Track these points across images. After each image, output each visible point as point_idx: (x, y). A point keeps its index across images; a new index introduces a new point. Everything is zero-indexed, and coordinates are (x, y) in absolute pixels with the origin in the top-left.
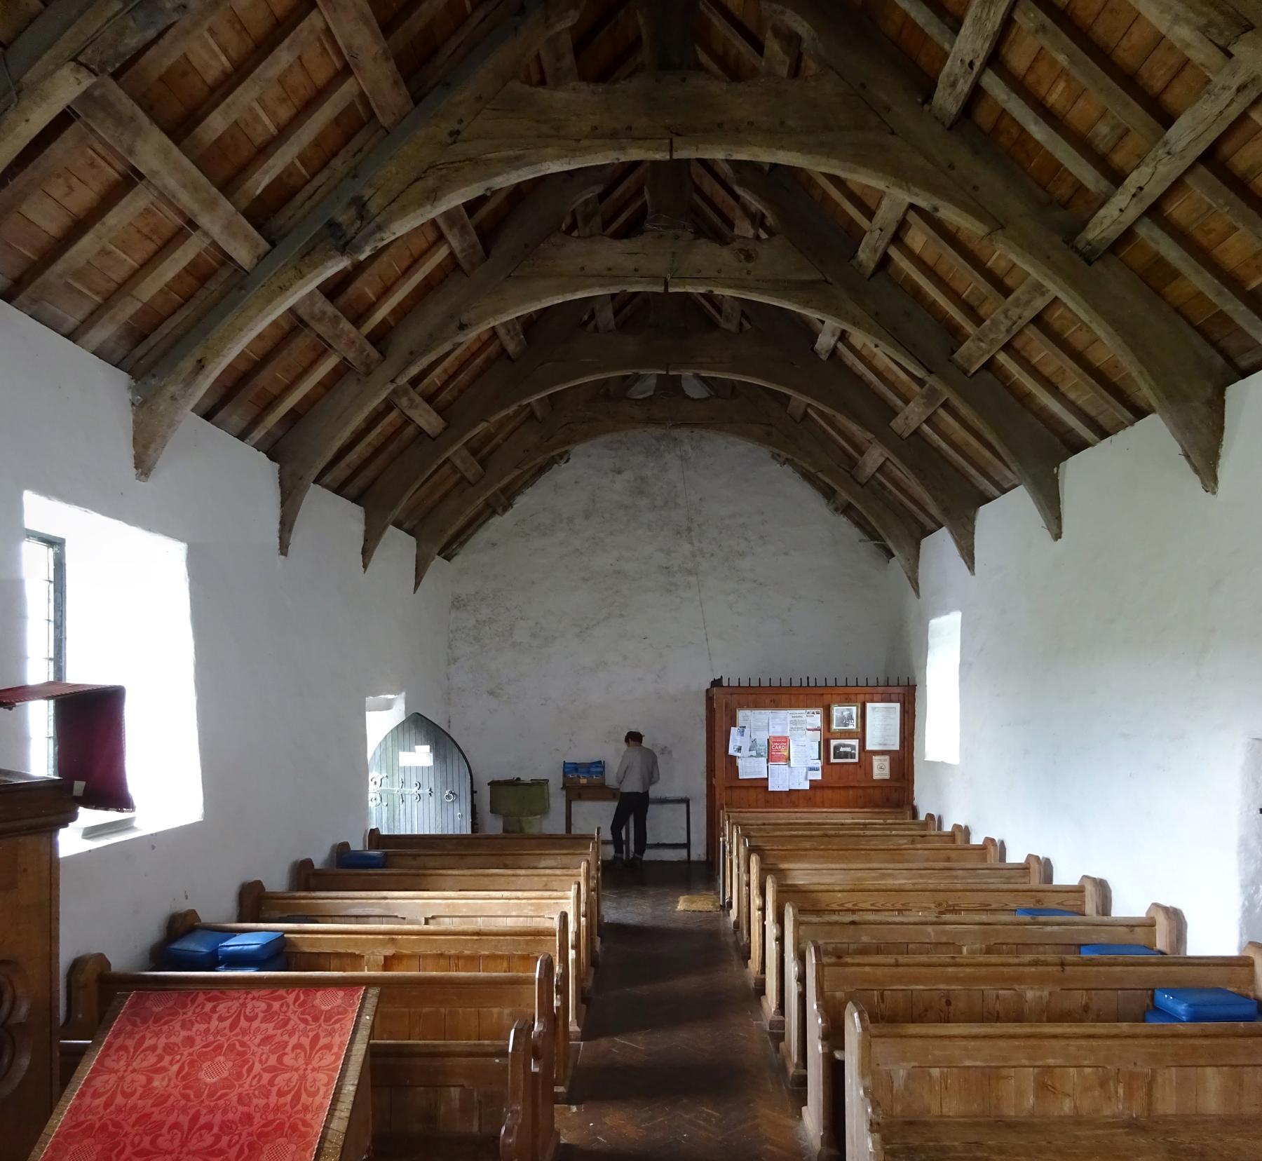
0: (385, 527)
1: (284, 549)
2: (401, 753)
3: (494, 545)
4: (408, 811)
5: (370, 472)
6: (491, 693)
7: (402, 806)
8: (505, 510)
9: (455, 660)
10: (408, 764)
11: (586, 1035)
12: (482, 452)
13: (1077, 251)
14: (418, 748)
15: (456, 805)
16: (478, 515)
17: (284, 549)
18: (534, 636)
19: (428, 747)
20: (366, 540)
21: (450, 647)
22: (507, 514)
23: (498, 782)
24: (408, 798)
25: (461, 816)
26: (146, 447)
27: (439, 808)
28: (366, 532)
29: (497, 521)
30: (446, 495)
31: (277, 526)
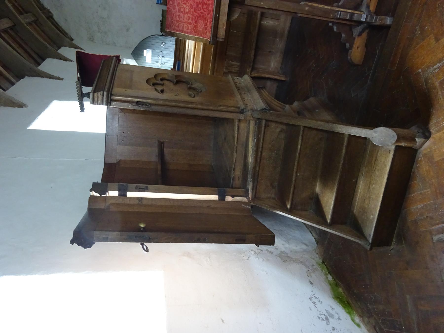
0: (58, 53)
1: (62, 79)
2: (146, 62)
3: (66, 20)
4: (167, 61)
5: (29, 51)
6: (128, 30)
7: (166, 64)
8: (50, 12)
9: (114, 43)
10: (151, 60)
11: (246, 195)
12: (22, 11)
13: (75, 47)
14: (145, 55)
15: (167, 42)
16: (53, 24)
17: (62, 79)
18: (105, 8)
19: (145, 51)
20: (61, 59)
21: (109, 44)
22: (52, 12)
23: (161, 29)
24: (163, 61)
25: (171, 41)
26: (14, 103)
27: (167, 50)
28: (57, 58)
29: (55, 17)
30: (43, 31)
31: (51, 80)
